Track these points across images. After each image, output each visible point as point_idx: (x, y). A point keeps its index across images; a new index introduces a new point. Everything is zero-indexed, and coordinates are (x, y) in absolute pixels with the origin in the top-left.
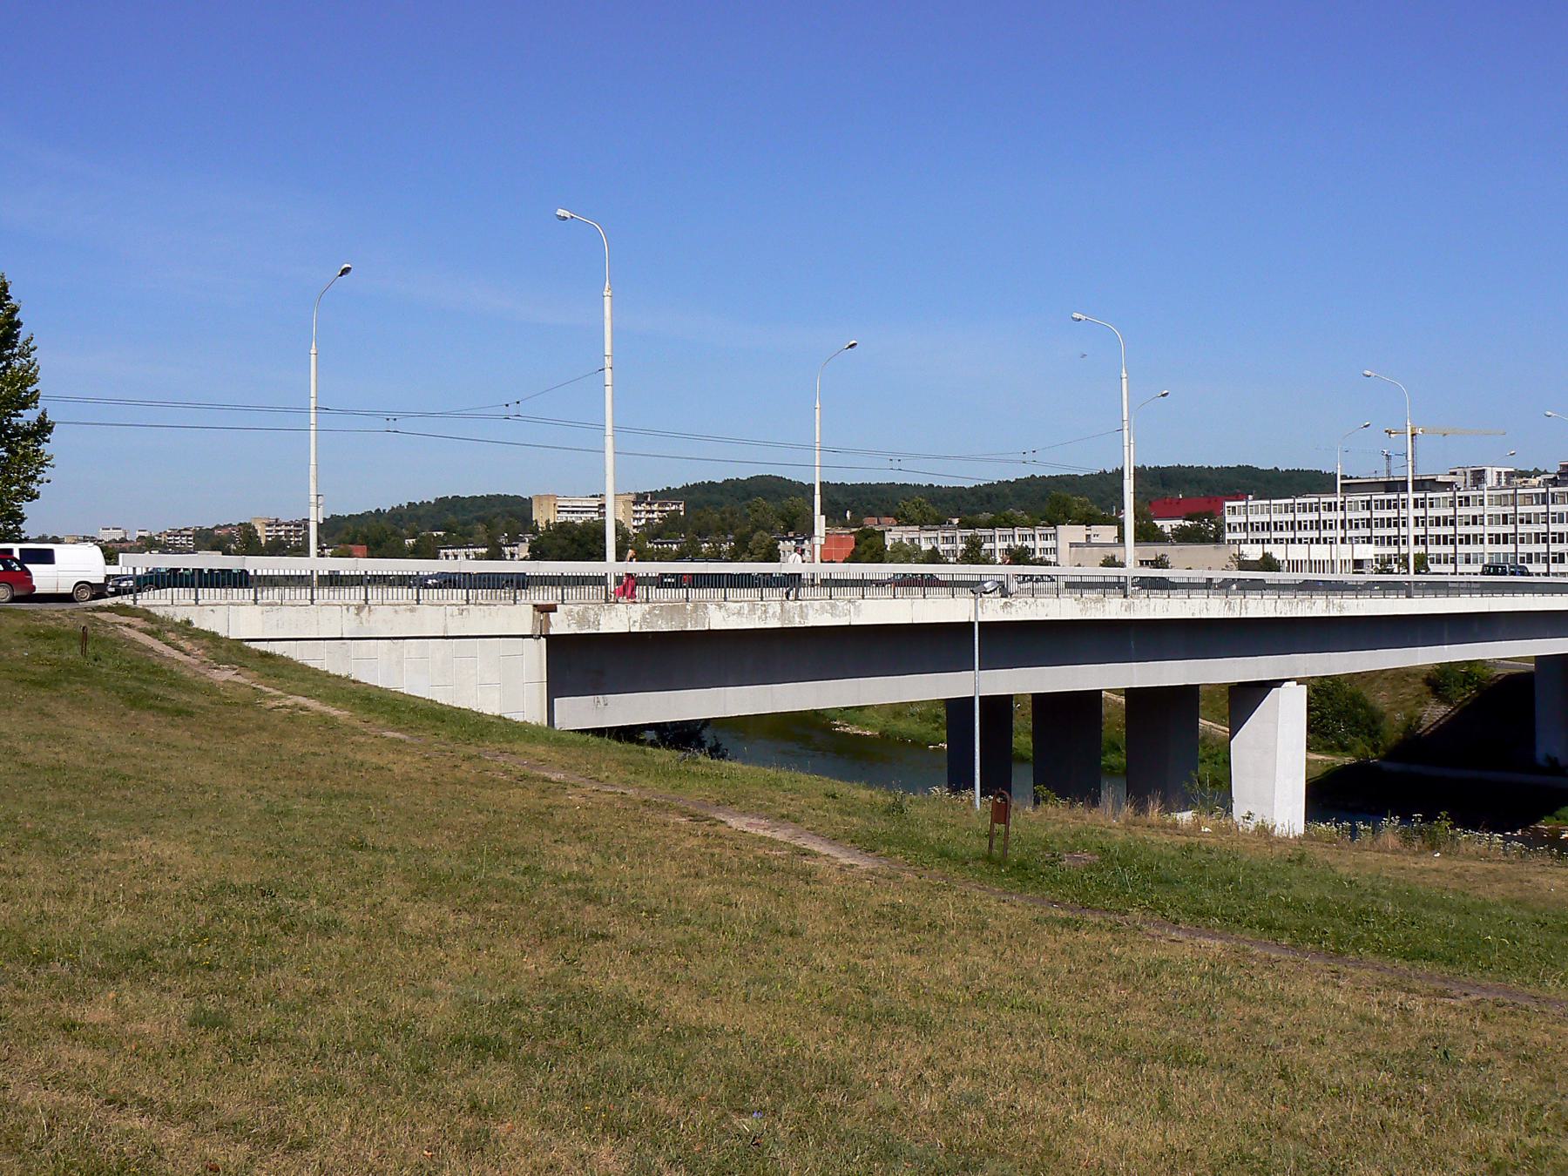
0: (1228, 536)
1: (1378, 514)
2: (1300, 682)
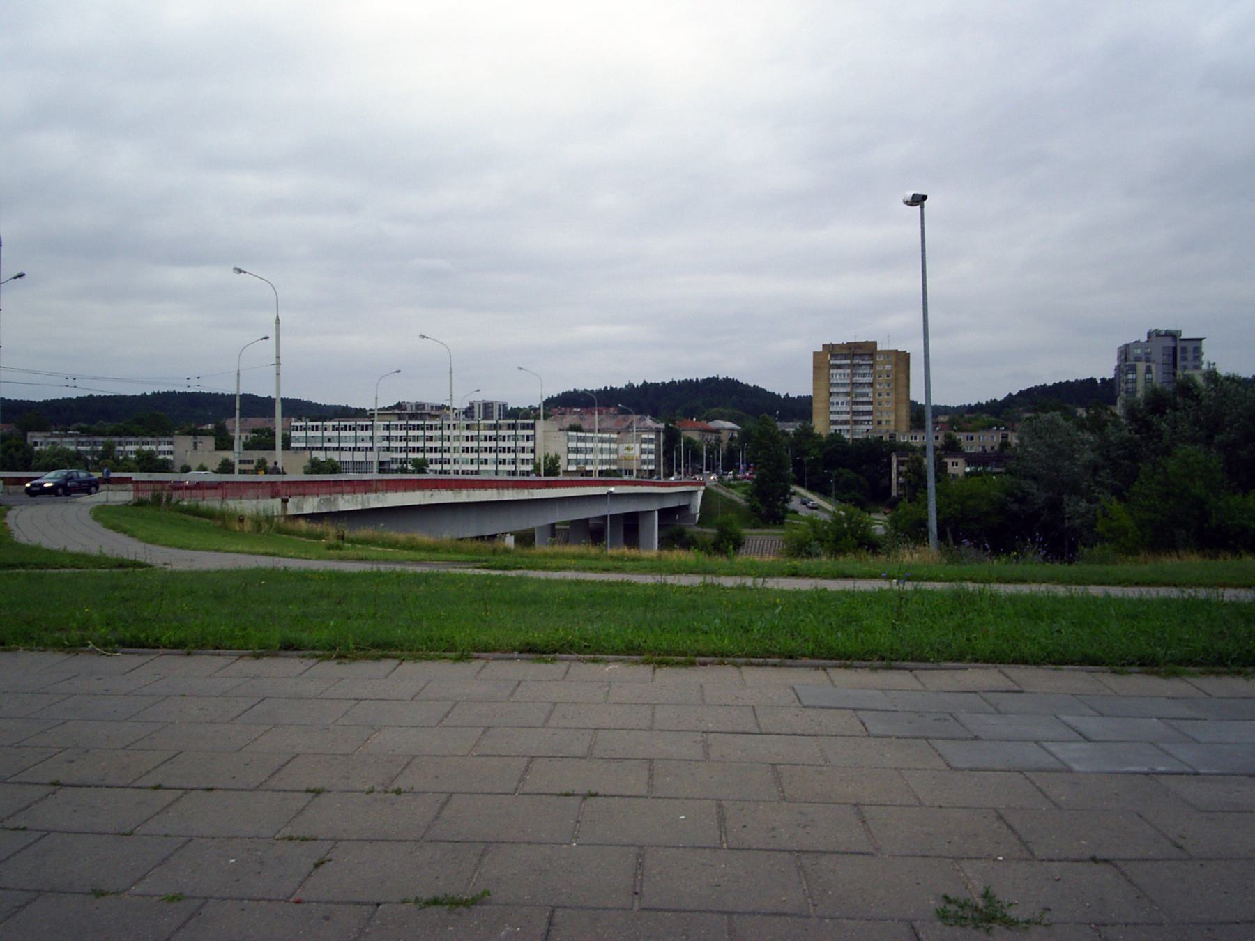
0: (293, 445)
1: (394, 433)
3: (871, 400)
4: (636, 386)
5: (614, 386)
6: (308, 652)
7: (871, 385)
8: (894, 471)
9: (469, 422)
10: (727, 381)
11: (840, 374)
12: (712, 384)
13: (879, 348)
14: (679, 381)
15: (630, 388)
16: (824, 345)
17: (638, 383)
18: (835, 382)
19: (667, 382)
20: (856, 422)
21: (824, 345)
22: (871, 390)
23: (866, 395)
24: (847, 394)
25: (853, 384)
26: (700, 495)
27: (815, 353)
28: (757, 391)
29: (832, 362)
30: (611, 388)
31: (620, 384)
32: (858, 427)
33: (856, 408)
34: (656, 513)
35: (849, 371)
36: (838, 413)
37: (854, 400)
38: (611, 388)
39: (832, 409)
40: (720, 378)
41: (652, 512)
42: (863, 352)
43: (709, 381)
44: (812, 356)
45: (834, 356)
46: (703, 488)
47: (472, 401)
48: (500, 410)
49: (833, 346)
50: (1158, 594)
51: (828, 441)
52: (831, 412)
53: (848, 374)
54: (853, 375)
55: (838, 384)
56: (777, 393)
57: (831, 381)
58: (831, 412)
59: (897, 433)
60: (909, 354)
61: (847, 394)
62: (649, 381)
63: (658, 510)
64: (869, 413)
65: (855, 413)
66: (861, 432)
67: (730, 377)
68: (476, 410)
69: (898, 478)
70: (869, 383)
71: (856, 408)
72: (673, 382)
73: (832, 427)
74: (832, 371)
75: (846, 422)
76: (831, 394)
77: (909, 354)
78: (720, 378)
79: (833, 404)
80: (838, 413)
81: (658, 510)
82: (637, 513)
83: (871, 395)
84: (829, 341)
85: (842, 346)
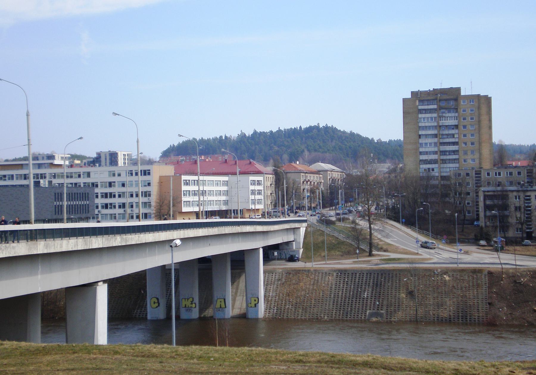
2: (104, 281)
3: (457, 140)
4: (247, 135)
5: (228, 135)
6: (215, 198)
7: (456, 127)
8: (481, 204)
9: (65, 177)
10: (327, 129)
11: (428, 118)
12: (262, 137)
13: (463, 93)
14: (213, 139)
15: (242, 137)
16: (412, 93)
17: (249, 132)
18: (423, 125)
19: (274, 130)
20: (444, 161)
21: (412, 93)
22: (457, 131)
23: (453, 136)
24: (436, 136)
25: (440, 126)
26: (303, 231)
27: (405, 100)
28: (353, 136)
29: (420, 107)
30: (226, 137)
31: (233, 133)
32: (445, 165)
33: (443, 148)
34: (261, 251)
35: (435, 115)
36: (426, 153)
37: (441, 141)
38: (226, 137)
39: (421, 150)
40: (321, 126)
41: (257, 249)
42: (448, 97)
43: (310, 129)
44: (455, 86)
45: (422, 101)
46: (305, 225)
47: (99, 151)
48: (124, 159)
49: (421, 92)
50: (444, 183)
51: (386, 160)
52: (421, 153)
53: (435, 118)
54: (440, 117)
55: (426, 127)
56: (370, 138)
57: (420, 125)
58: (421, 153)
59: (482, 170)
60: (491, 97)
61: (436, 136)
62: (258, 131)
63: (262, 247)
64: (455, 152)
65: (444, 153)
66: (449, 169)
67: (330, 125)
68: (103, 159)
69: (485, 211)
70: (455, 125)
71: (443, 148)
72: (279, 131)
73: (421, 166)
74: (420, 116)
75: (435, 162)
76: (420, 136)
77: (491, 97)
78: (321, 126)
79: (421, 144)
80: (426, 153)
81: (262, 247)
82: (242, 253)
83: (456, 136)
84: (416, 90)
85: (428, 93)
